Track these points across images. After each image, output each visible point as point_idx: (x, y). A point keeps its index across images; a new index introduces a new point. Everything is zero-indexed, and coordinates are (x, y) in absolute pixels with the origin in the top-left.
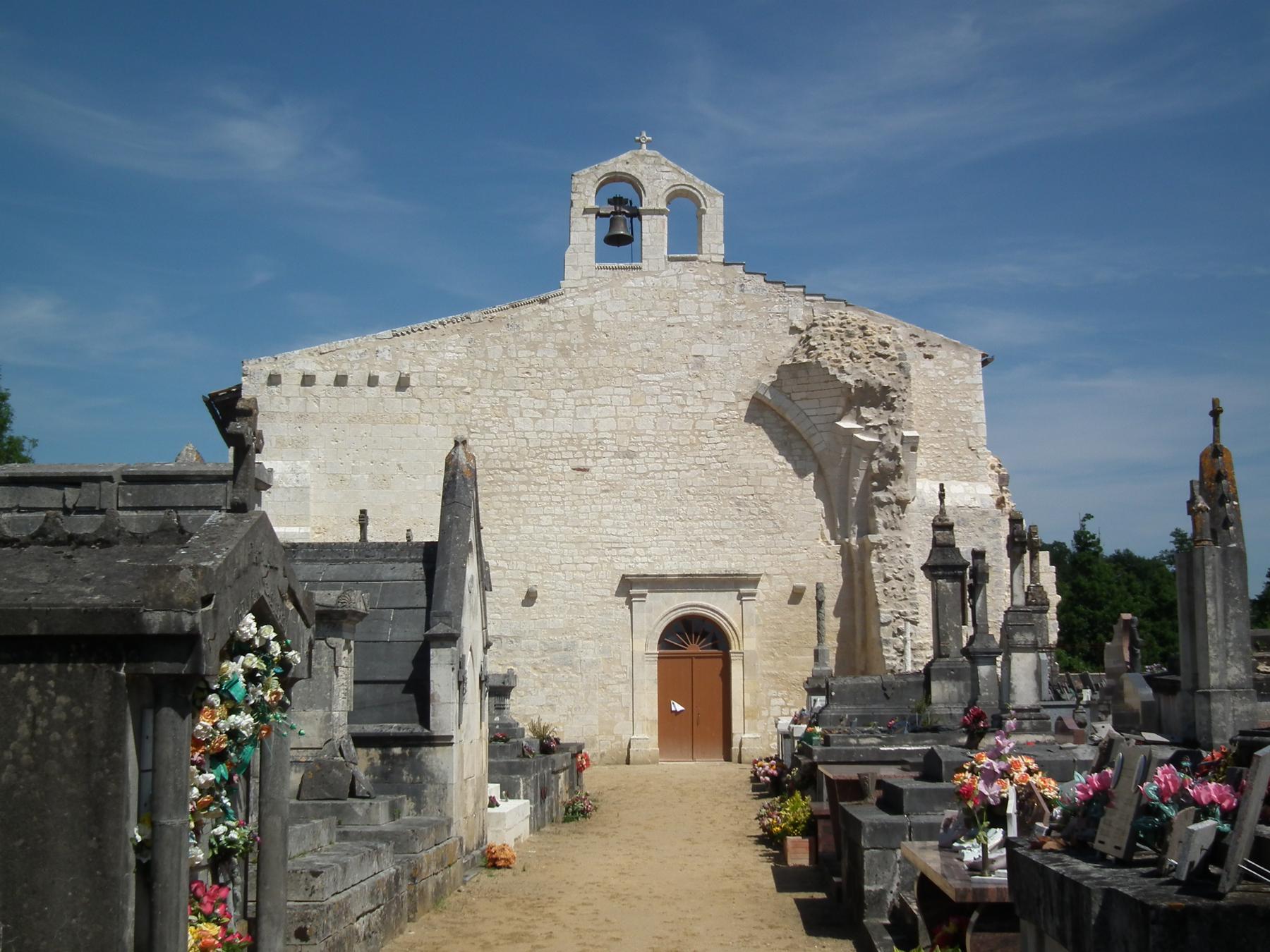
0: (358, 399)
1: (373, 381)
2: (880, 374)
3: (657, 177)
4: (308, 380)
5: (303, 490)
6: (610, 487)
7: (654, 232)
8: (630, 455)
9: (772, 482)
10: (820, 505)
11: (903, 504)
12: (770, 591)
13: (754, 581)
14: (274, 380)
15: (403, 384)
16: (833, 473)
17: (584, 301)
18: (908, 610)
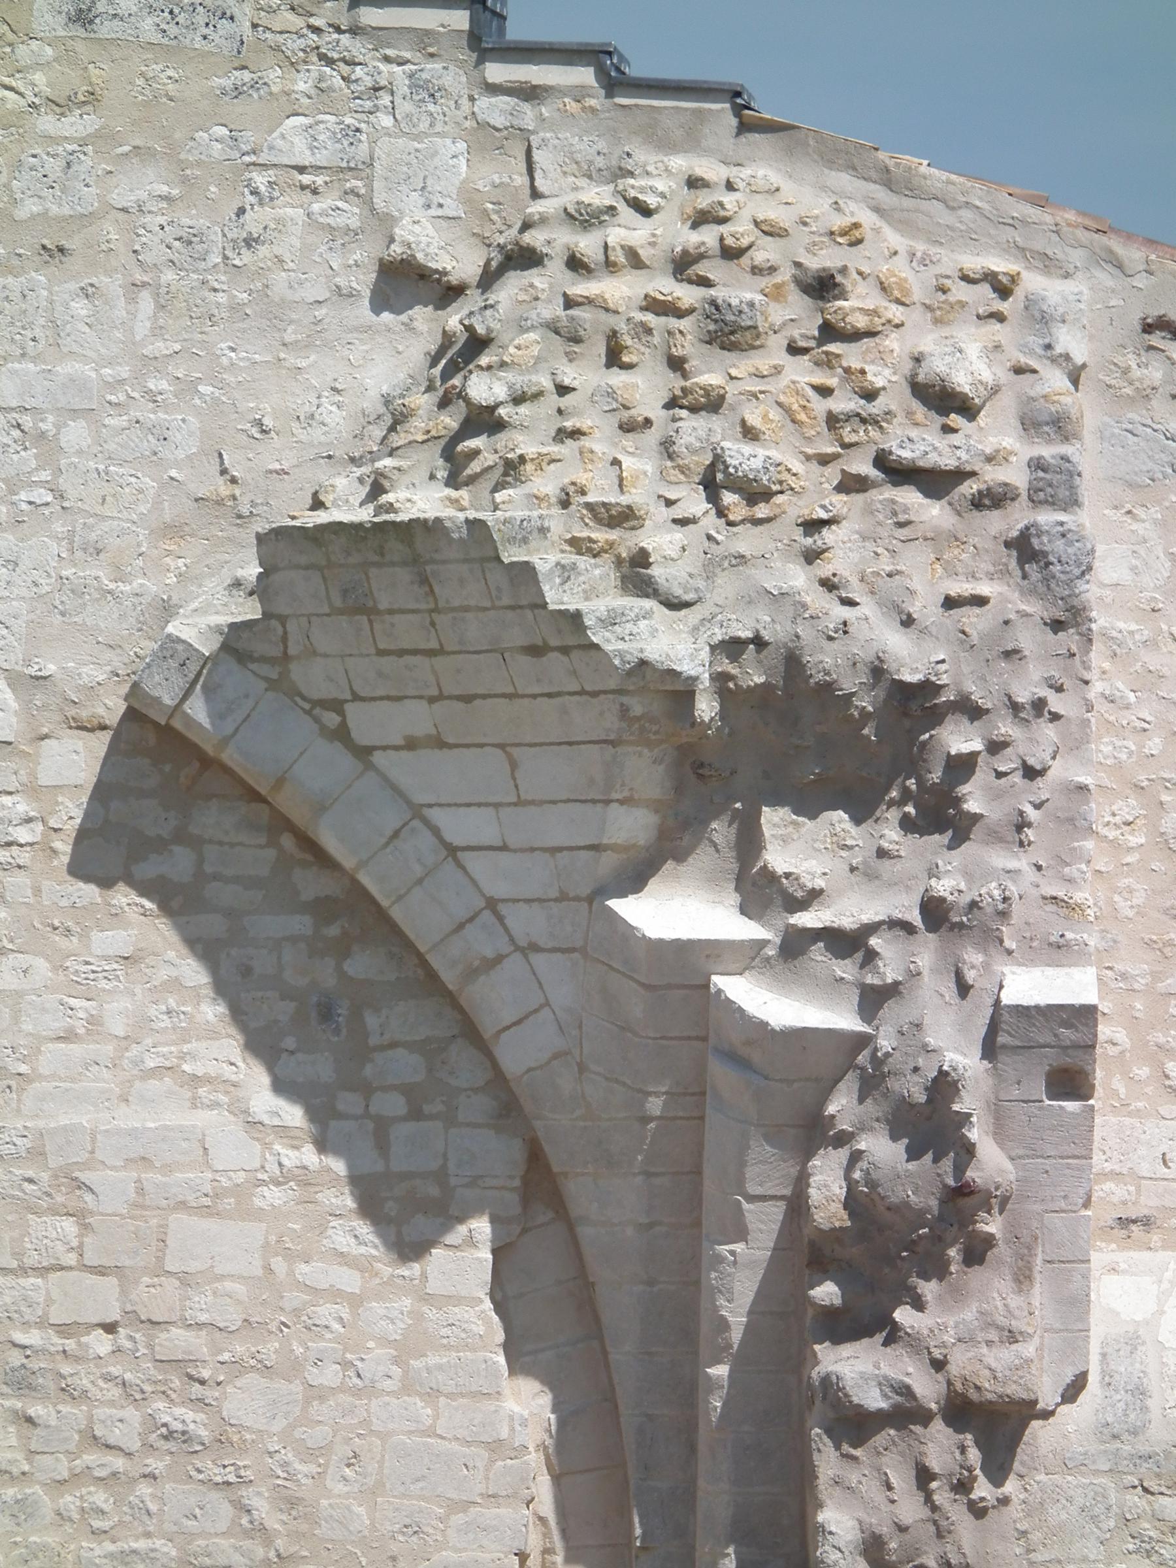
2: (886, 602)
11: (996, 1425)
16: (610, 1206)
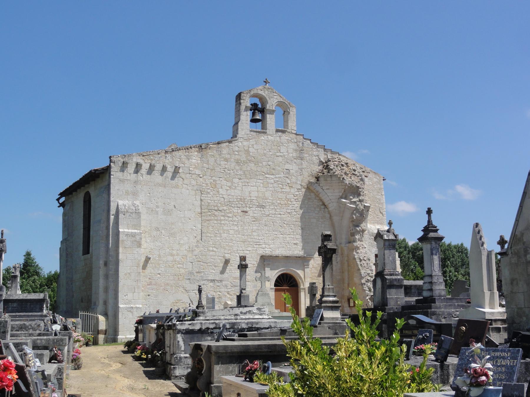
6: (255, 219)
8: (263, 207)
11: (363, 231)
17: (245, 143)
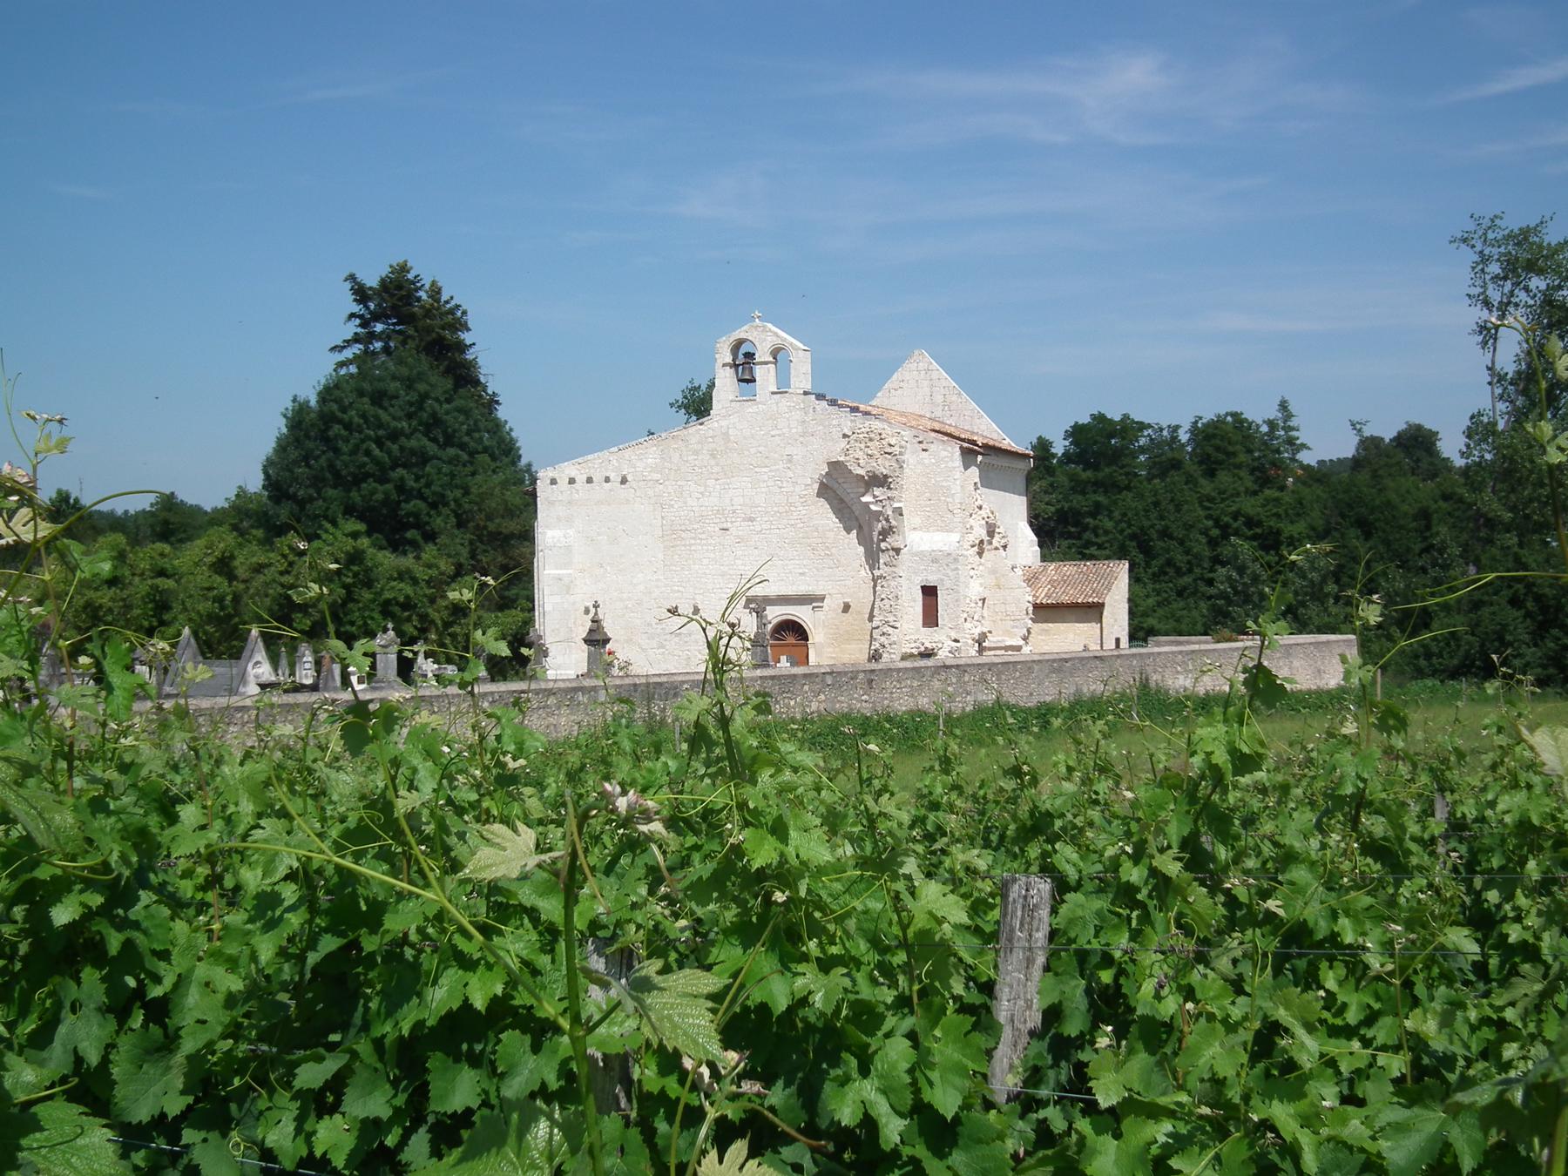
0: (600, 489)
1: (607, 480)
2: (883, 467)
3: (764, 337)
4: (572, 481)
5: (568, 548)
6: (740, 540)
7: (765, 375)
8: (751, 520)
9: (831, 535)
10: (862, 549)
11: (897, 551)
12: (832, 604)
13: (822, 599)
14: (553, 482)
15: (624, 481)
16: (866, 528)
17: (724, 423)
18: (891, 619)
